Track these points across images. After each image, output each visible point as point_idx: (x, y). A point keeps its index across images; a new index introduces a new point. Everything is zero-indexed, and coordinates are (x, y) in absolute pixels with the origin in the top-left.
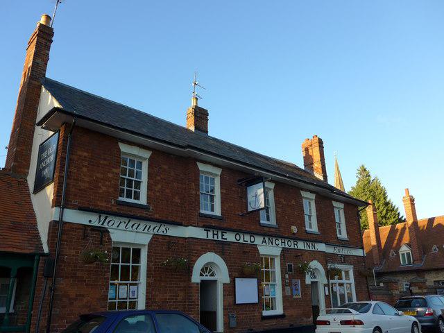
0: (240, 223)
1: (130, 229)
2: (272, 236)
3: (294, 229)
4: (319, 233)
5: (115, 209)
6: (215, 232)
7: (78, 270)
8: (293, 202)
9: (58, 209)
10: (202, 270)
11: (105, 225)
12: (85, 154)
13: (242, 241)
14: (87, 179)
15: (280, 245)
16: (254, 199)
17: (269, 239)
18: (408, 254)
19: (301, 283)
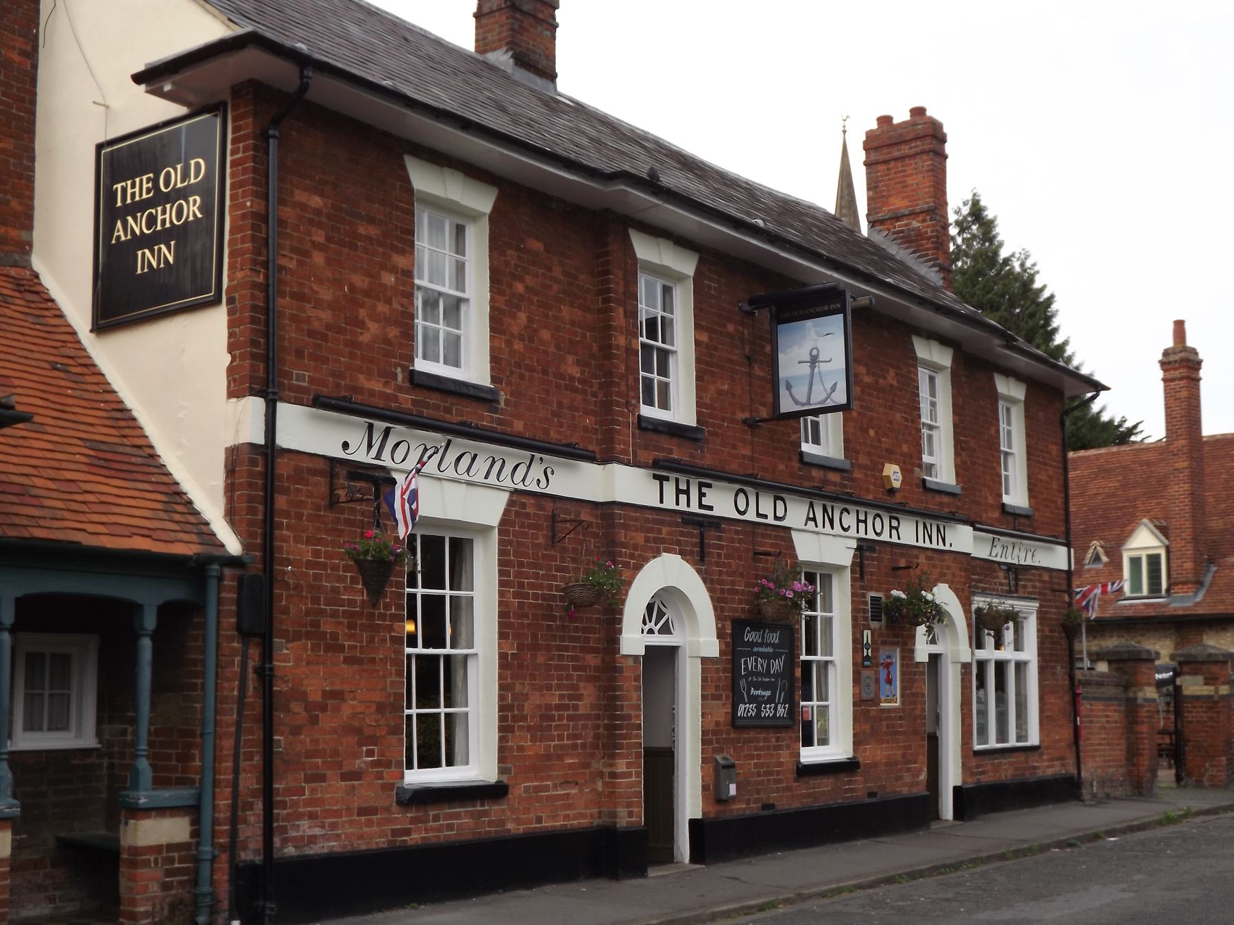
0: (748, 453)
1: (451, 473)
2: (836, 499)
3: (893, 473)
4: (958, 491)
5: (406, 400)
6: (862, 517)
7: (322, 612)
8: (891, 378)
9: (254, 406)
10: (650, 608)
11: (386, 461)
12: (316, 201)
13: (751, 516)
14: (326, 294)
15: (852, 532)
16: (805, 369)
17: (825, 510)
18: (1154, 560)
19: (902, 658)
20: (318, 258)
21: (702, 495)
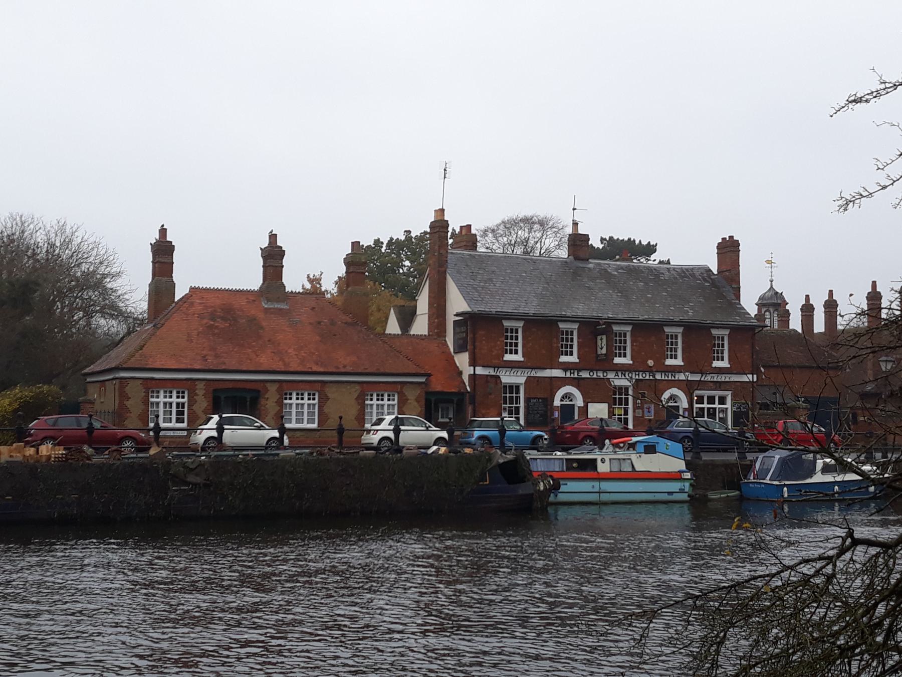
1: (512, 374)
9: (472, 368)
11: (498, 374)
20: (484, 342)
21: (578, 373)
